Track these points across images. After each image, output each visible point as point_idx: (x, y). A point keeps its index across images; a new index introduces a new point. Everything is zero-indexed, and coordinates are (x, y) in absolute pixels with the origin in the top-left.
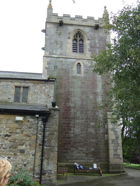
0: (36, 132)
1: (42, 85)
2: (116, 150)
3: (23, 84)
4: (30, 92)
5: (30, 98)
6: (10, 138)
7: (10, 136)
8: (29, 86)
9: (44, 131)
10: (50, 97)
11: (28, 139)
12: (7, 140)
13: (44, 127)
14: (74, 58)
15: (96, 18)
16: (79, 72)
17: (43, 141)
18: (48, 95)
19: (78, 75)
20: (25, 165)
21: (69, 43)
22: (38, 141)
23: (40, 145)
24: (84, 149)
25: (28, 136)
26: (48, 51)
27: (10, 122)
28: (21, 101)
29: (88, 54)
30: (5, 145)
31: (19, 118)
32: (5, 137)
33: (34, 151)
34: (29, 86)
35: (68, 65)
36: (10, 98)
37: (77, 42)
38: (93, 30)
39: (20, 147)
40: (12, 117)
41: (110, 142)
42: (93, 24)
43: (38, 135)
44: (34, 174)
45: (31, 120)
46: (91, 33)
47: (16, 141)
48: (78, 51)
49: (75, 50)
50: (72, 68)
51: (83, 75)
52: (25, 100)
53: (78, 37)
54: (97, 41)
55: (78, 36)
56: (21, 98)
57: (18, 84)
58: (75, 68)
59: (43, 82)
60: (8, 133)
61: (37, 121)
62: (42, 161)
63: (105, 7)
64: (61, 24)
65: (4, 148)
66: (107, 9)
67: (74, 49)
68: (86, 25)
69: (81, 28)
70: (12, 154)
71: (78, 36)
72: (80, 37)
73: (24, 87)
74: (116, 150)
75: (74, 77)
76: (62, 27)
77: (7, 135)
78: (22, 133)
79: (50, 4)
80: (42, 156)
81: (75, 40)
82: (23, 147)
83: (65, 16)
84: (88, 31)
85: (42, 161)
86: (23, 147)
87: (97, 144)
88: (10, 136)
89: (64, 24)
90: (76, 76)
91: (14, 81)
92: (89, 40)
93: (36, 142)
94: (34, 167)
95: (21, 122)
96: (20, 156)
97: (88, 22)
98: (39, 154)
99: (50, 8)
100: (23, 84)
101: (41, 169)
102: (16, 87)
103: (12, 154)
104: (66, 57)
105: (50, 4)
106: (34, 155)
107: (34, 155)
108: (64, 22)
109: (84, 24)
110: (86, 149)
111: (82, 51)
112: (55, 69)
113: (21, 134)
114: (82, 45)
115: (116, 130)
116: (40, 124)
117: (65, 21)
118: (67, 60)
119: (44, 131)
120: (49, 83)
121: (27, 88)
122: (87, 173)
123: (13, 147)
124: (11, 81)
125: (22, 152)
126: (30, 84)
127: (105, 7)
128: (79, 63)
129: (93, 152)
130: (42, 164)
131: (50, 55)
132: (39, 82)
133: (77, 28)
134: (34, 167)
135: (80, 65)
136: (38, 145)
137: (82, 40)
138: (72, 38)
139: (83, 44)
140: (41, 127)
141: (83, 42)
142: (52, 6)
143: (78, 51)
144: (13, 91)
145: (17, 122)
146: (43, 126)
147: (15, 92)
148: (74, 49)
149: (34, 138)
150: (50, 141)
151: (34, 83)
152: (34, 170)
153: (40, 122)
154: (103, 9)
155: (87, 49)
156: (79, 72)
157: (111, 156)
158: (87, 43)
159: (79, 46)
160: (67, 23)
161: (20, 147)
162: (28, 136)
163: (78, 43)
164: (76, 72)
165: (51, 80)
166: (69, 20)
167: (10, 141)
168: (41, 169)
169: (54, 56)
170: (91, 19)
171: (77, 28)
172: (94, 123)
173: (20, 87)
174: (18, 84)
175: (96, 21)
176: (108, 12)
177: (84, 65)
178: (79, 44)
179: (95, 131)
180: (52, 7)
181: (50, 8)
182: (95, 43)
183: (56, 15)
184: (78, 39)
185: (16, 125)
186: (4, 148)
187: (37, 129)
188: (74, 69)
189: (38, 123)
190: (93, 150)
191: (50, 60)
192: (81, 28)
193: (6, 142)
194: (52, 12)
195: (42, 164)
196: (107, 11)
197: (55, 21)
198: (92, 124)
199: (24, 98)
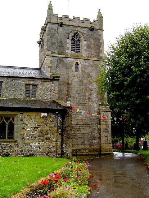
3: (32, 82)
4: (39, 89)
6: (38, 130)
7: (38, 128)
8: (38, 84)
10: (55, 94)
11: (51, 129)
12: (36, 131)
13: (63, 121)
15: (92, 20)
16: (77, 70)
18: (54, 92)
20: (50, 149)
21: (68, 44)
26: (50, 51)
27: (38, 117)
28: (31, 97)
31: (46, 115)
32: (35, 128)
34: (38, 84)
36: (22, 95)
37: (74, 42)
38: (89, 31)
39: (46, 136)
40: (39, 113)
42: (90, 26)
44: (57, 155)
45: (52, 116)
47: (43, 131)
48: (76, 50)
49: (73, 50)
51: (81, 73)
52: (34, 95)
53: (76, 37)
57: (28, 82)
59: (49, 81)
60: (36, 126)
61: (57, 117)
62: (62, 145)
63: (99, 10)
65: (35, 137)
66: (101, 11)
67: (72, 50)
69: (78, 29)
72: (77, 38)
73: (33, 85)
78: (47, 126)
80: (62, 142)
81: (73, 39)
82: (49, 136)
84: (85, 32)
85: (62, 145)
86: (49, 136)
88: (38, 128)
89: (64, 25)
91: (24, 79)
92: (85, 40)
94: (57, 150)
95: (46, 117)
96: (47, 143)
98: (60, 140)
99: (50, 9)
100: (32, 82)
101: (62, 151)
102: (26, 85)
104: (66, 56)
106: (56, 141)
107: (56, 141)
109: (81, 25)
111: (79, 50)
112: (57, 67)
113: (46, 126)
114: (79, 45)
115: (107, 121)
116: (59, 118)
117: (65, 22)
120: (55, 81)
121: (36, 85)
125: (48, 139)
126: (38, 82)
127: (99, 10)
128: (77, 63)
130: (62, 148)
132: (46, 80)
133: (75, 28)
134: (57, 150)
135: (78, 64)
136: (58, 133)
137: (79, 40)
138: (70, 38)
139: (80, 44)
140: (60, 121)
141: (80, 42)
144: (24, 89)
145: (43, 117)
147: (26, 90)
148: (72, 50)
151: (41, 81)
152: (57, 152)
153: (59, 117)
156: (77, 70)
157: (103, 142)
158: (83, 43)
159: (77, 46)
161: (46, 136)
163: (76, 42)
164: (74, 70)
165: (56, 78)
166: (68, 21)
168: (62, 151)
170: (87, 20)
173: (30, 85)
174: (28, 82)
175: (91, 23)
178: (77, 44)
181: (50, 9)
183: (56, 16)
184: (76, 39)
185: (42, 120)
186: (35, 137)
188: (73, 68)
189: (58, 118)
192: (78, 29)
195: (62, 148)
199: (33, 93)
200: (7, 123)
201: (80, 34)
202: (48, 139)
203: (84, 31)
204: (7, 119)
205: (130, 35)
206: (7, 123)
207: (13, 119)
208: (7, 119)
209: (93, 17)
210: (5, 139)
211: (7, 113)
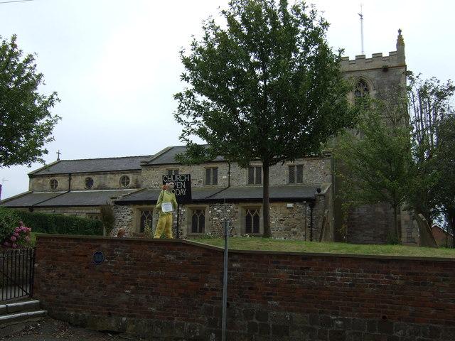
1: (316, 161)
2: (410, 233)
4: (305, 172)
5: (305, 178)
9: (311, 215)
15: (386, 54)
17: (311, 224)
24: (371, 232)
27: (283, 208)
28: (296, 182)
31: (290, 205)
41: (403, 222)
46: (378, 79)
55: (361, 84)
56: (296, 178)
63: (400, 31)
69: (364, 74)
71: (361, 84)
74: (410, 233)
84: (373, 77)
87: (387, 226)
119: (311, 215)
121: (302, 166)
122: (254, 222)
123: (288, 229)
125: (295, 233)
127: (400, 31)
150: (317, 224)
171: (358, 75)
185: (288, 211)
190: (382, 232)
192: (364, 74)
200: (198, 217)
201: (367, 81)
202: (295, 233)
203: (372, 75)
204: (253, 211)
205: (33, 83)
206: (198, 217)
207: (204, 211)
208: (253, 211)
209: (388, 48)
210: (196, 232)
211: (251, 204)
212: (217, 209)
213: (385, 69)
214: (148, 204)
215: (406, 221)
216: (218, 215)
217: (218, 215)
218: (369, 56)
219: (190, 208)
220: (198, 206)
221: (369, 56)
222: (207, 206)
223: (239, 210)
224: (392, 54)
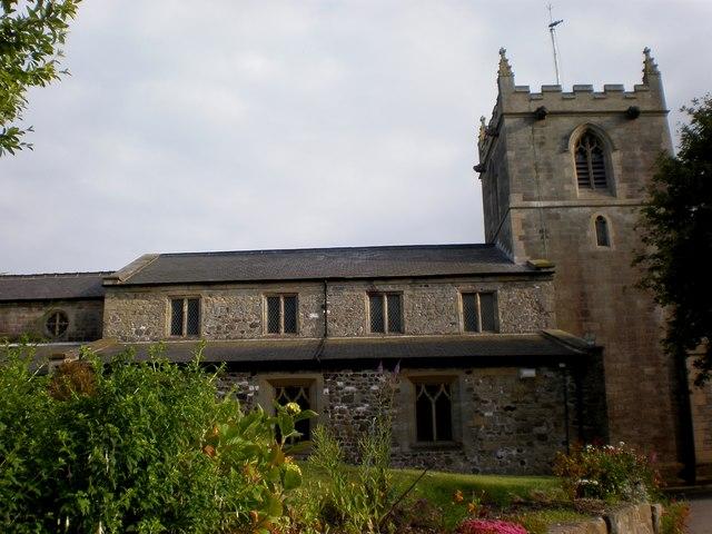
0: (563, 398)
4: (501, 304)
6: (514, 413)
14: (585, 204)
16: (603, 241)
19: (603, 248)
22: (570, 416)
23: (574, 423)
25: (548, 406)
29: (621, 188)
30: (508, 426)
31: (529, 373)
33: (564, 436)
35: (572, 223)
39: (537, 430)
42: (624, 106)
43: (569, 404)
45: (551, 374)
48: (593, 181)
50: (584, 231)
54: (638, 152)
55: (587, 140)
57: (469, 287)
58: (592, 233)
59: (527, 279)
60: (509, 404)
63: (502, 52)
64: (540, 115)
65: (507, 433)
68: (604, 109)
70: (524, 443)
75: (594, 256)
76: (541, 122)
77: (508, 408)
79: (504, 62)
82: (543, 429)
83: (546, 90)
86: (543, 429)
90: (598, 252)
93: (567, 419)
95: (532, 379)
96: (540, 448)
97: (610, 101)
99: (505, 73)
103: (524, 443)
104: (567, 203)
105: (504, 62)
108: (549, 109)
110: (639, 432)
112: (542, 238)
117: (552, 105)
118: (570, 210)
124: (451, 280)
125: (542, 438)
127: (502, 52)
128: (600, 218)
129: (655, 438)
131: (526, 203)
132: (517, 278)
136: (570, 423)
137: (598, 152)
141: (602, 157)
142: (512, 75)
143: (593, 181)
145: (525, 380)
146: (575, 386)
149: (561, 409)
153: (569, 378)
154: (643, 58)
155: (616, 177)
156: (603, 241)
160: (555, 109)
161: (537, 430)
162: (548, 406)
167: (517, 419)
169: (535, 204)
172: (654, 369)
174: (469, 287)
175: (627, 97)
176: (656, 66)
177: (613, 222)
179: (656, 388)
180: (512, 70)
181: (505, 73)
182: (634, 157)
183: (524, 91)
187: (565, 392)
188: (589, 234)
189: (565, 381)
191: (528, 216)
193: (509, 421)
194: (512, 83)
196: (655, 62)
197: (525, 109)
198: (648, 370)
200: (433, 401)
202: (542, 438)
204: (433, 389)
206: (433, 401)
209: (631, 80)
211: (432, 372)
212: (346, 384)
213: (632, 114)
214: (292, 371)
215: (700, 407)
216: (348, 399)
217: (348, 399)
218: (567, 88)
219: (270, 382)
220: (295, 376)
221: (567, 88)
222: (319, 377)
223: (407, 388)
224: (637, 89)
